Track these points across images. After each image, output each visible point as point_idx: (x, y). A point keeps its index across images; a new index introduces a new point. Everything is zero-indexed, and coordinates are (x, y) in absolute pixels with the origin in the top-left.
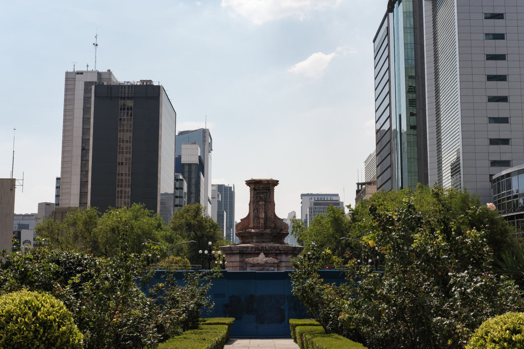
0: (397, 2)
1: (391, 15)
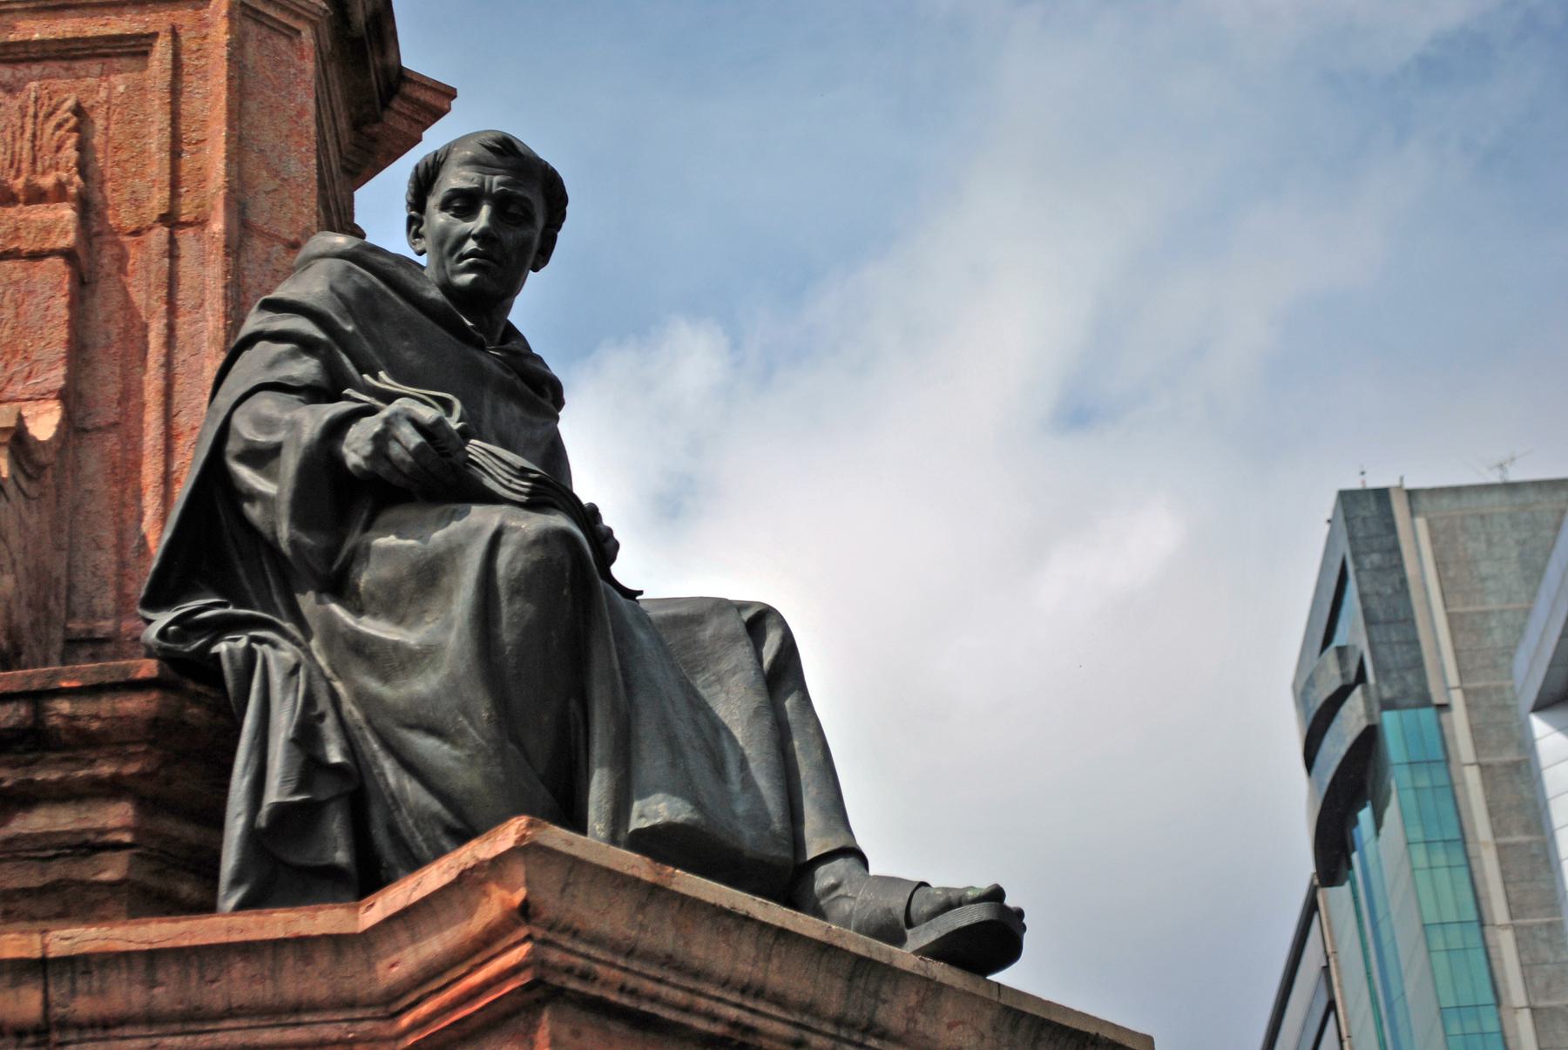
0: (1365, 815)
1: (1337, 899)
